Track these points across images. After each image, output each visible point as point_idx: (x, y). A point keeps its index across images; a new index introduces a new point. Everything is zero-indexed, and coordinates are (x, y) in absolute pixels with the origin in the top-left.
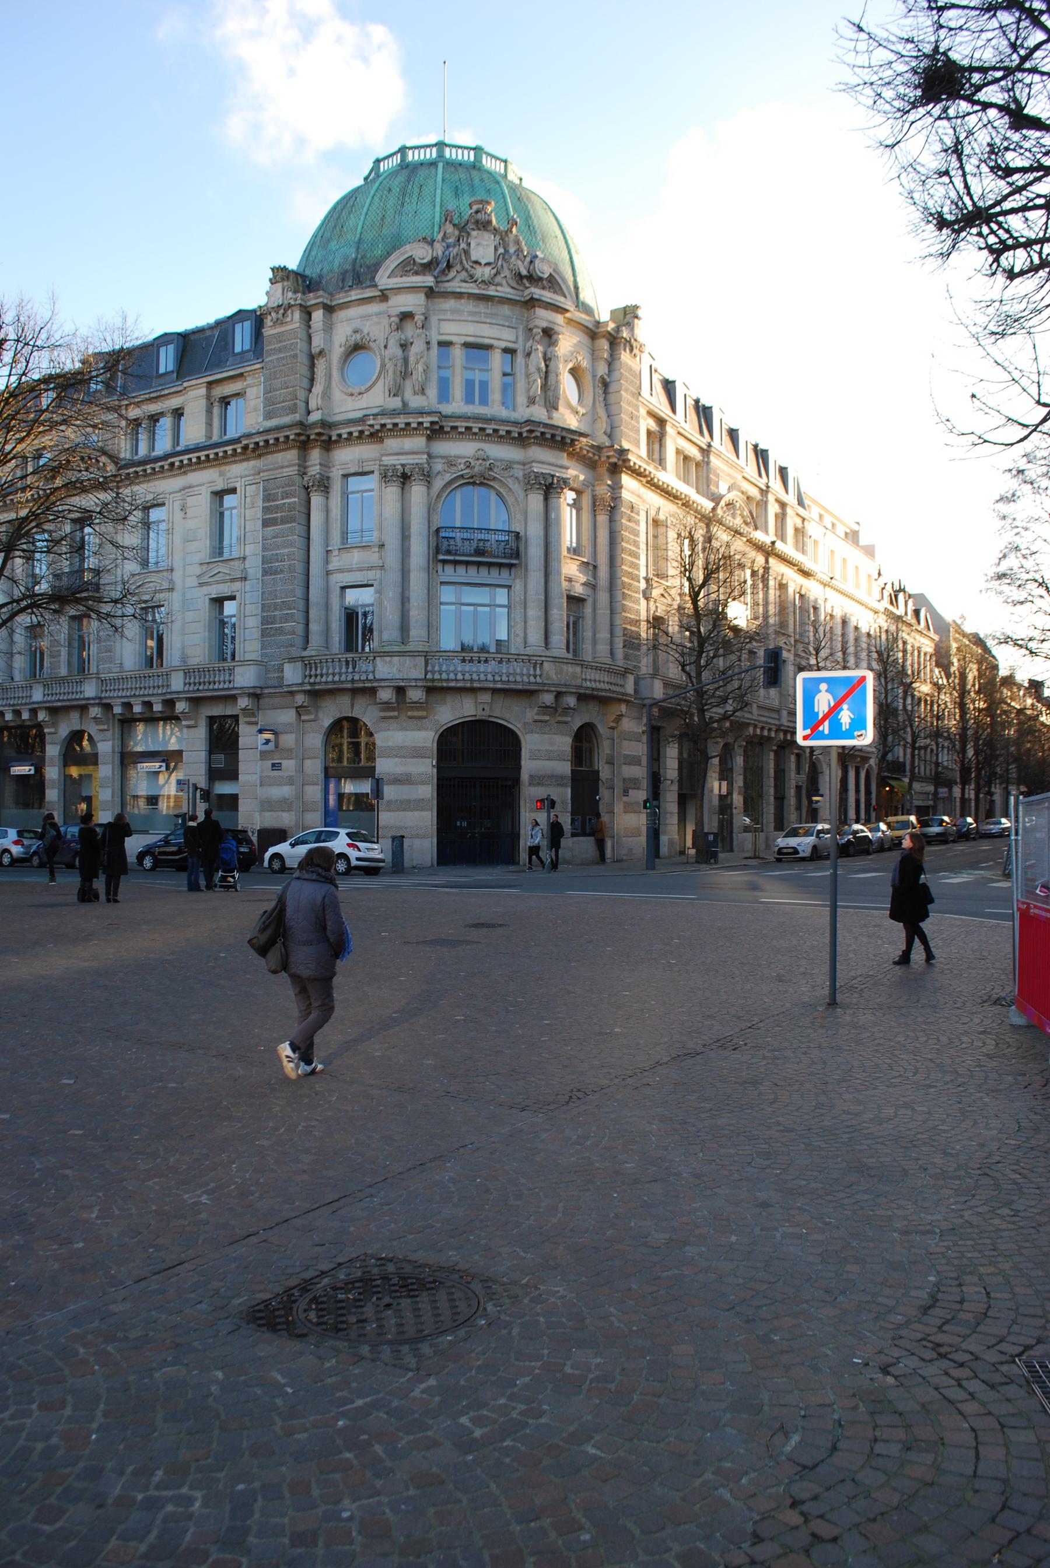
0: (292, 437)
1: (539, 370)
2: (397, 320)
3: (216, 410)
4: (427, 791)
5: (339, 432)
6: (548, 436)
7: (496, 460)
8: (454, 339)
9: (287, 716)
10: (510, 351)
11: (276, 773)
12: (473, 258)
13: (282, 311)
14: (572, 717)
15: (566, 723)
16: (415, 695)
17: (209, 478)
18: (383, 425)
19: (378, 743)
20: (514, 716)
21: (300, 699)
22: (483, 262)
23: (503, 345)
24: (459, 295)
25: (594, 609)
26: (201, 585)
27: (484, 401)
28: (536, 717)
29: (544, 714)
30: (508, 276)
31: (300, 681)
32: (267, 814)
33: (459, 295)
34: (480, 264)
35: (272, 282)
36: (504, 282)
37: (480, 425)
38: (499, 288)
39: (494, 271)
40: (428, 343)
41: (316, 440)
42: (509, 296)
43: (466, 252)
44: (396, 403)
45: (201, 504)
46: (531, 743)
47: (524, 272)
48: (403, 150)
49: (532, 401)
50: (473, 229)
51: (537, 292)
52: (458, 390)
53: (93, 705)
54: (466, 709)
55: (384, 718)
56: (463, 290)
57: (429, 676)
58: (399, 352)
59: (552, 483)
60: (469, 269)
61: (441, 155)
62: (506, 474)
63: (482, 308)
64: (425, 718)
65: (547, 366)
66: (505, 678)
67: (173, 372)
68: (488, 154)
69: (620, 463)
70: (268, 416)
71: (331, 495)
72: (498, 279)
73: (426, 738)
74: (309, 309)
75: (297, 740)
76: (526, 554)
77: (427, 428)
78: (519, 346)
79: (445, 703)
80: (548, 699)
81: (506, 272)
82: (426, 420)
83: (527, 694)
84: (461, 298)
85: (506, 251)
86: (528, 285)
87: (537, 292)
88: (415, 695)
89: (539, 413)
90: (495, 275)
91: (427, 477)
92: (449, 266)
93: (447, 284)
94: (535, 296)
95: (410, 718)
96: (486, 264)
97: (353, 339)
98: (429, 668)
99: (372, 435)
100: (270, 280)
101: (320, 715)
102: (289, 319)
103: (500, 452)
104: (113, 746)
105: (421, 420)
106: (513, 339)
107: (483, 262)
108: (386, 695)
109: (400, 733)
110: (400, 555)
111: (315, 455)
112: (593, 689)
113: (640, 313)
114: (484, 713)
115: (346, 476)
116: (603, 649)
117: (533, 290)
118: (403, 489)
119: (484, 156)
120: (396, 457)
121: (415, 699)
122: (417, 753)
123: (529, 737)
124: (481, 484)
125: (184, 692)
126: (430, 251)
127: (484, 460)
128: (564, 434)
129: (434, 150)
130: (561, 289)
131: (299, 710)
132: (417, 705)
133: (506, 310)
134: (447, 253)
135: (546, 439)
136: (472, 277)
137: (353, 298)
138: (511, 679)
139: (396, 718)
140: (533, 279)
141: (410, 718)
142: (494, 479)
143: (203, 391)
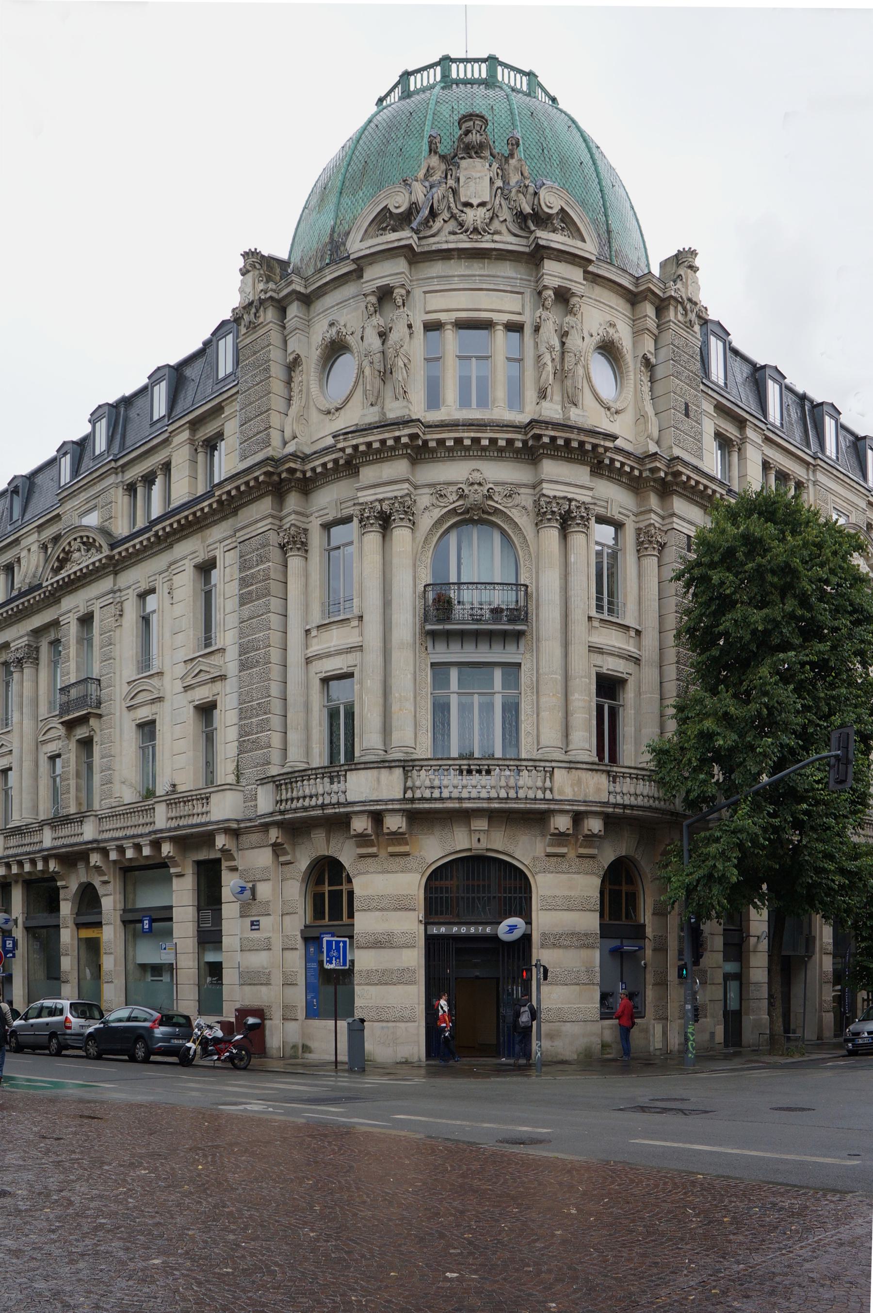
0: (261, 478)
1: (551, 349)
2: (373, 299)
3: (201, 457)
4: (414, 958)
5: (312, 465)
6: (560, 442)
7: (496, 484)
8: (443, 317)
9: (263, 858)
10: (515, 328)
11: (255, 935)
12: (463, 199)
13: (253, 310)
14: (598, 848)
15: (407, 854)
16: (394, 823)
17: (191, 550)
18: (355, 447)
19: (357, 892)
20: (524, 850)
21: (274, 834)
22: (475, 202)
23: (505, 318)
24: (446, 255)
25: (639, 693)
26: (187, 688)
27: (483, 403)
28: (550, 850)
29: (560, 845)
30: (509, 219)
31: (271, 810)
32: (247, 988)
33: (446, 255)
34: (471, 205)
35: (244, 272)
36: (503, 229)
37: (473, 435)
38: (496, 237)
39: (489, 215)
40: (410, 326)
41: (290, 480)
42: (510, 247)
43: (455, 192)
44: (371, 416)
45: (185, 581)
46: (545, 885)
47: (528, 210)
48: (446, 61)
49: (543, 394)
50: (463, 158)
51: (546, 237)
52: (451, 393)
53: (93, 849)
54: (461, 841)
55: (362, 856)
56: (451, 246)
57: (409, 795)
58: (376, 342)
59: (569, 511)
60: (459, 214)
61: (445, 76)
62: (510, 502)
63: (477, 268)
64: (407, 854)
65: (563, 344)
66: (503, 794)
67: (164, 416)
68: (507, 66)
69: (669, 478)
70: (243, 458)
71: (309, 555)
72: (496, 225)
73: (410, 883)
74: (284, 304)
75: (273, 890)
76: (537, 615)
77: (406, 446)
78: (527, 319)
79: (433, 833)
80: (562, 823)
81: (505, 214)
82: (404, 433)
83: (533, 818)
84: (449, 258)
85: (506, 182)
86: (533, 228)
87: (546, 237)
88: (394, 823)
89: (552, 410)
90: (491, 219)
91: (409, 513)
92: (433, 214)
93: (432, 240)
94: (542, 242)
95: (392, 855)
96: (478, 206)
97: (328, 335)
98: (409, 784)
99: (348, 463)
100: (241, 270)
101: (298, 854)
102: (261, 320)
103: (498, 473)
104: (115, 902)
105: (397, 434)
106: (518, 308)
107: (475, 202)
108: (360, 825)
109: (381, 877)
110: (382, 628)
111: (293, 501)
112: (625, 807)
113: (698, 262)
114: (479, 846)
115: (327, 527)
116: (551, 735)
117: (539, 233)
118: (384, 537)
119: (499, 69)
120: (372, 491)
121: (394, 828)
122: (401, 906)
123: (540, 878)
124: (481, 522)
125: (169, 830)
126: (407, 195)
127: (480, 484)
128: (582, 438)
129: (438, 69)
130: (578, 230)
131: (277, 849)
132: (397, 837)
133: (507, 270)
134: (429, 196)
135: (558, 448)
136: (461, 225)
137: (328, 278)
138: (512, 794)
139: (374, 856)
140: (541, 219)
141: (392, 855)
142: (497, 511)
143: (186, 435)
